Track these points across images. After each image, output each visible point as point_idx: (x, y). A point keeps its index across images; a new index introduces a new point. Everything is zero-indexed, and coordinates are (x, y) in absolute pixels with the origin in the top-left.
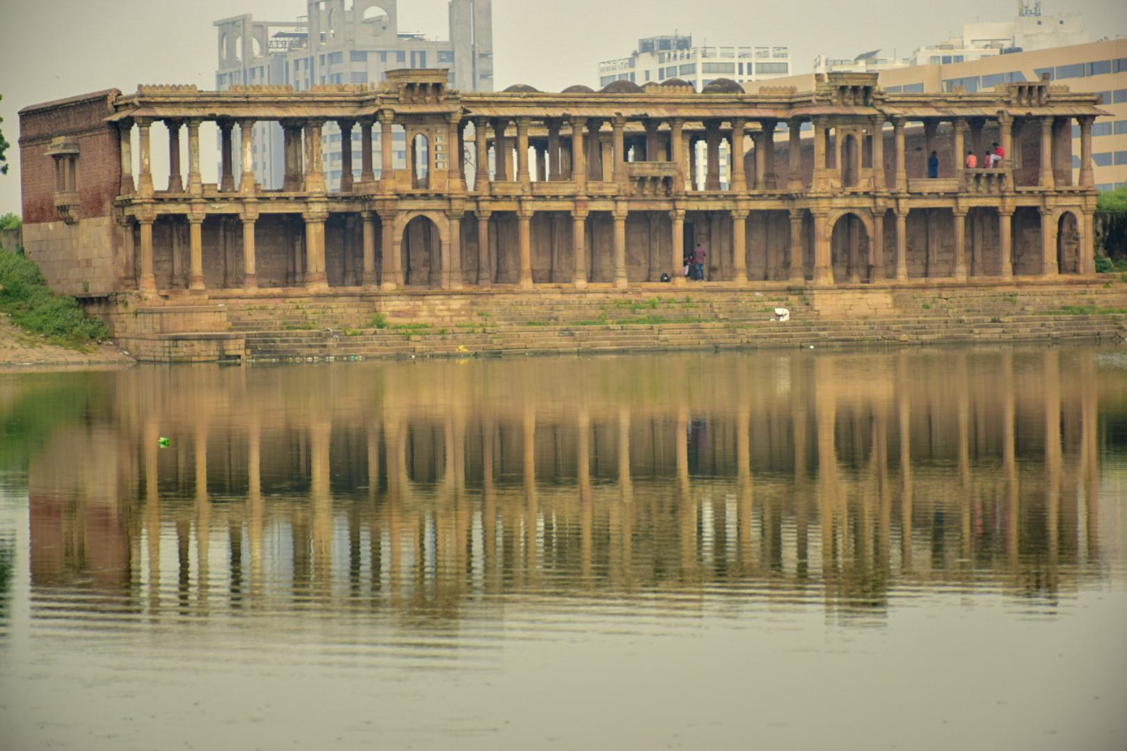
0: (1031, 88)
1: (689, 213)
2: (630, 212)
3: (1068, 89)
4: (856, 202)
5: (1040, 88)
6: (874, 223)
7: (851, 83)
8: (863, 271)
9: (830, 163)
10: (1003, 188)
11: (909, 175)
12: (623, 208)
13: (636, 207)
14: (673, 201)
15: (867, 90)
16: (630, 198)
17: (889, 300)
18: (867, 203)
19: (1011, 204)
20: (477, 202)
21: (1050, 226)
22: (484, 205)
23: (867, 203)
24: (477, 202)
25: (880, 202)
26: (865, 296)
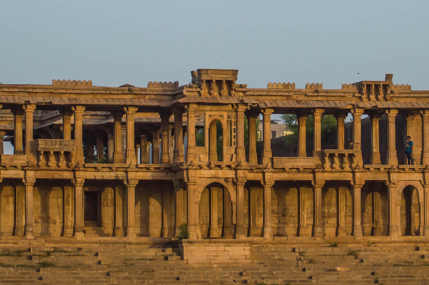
0: (377, 87)
1: (88, 182)
2: (37, 180)
3: (410, 87)
4: (220, 173)
5: (385, 87)
6: (237, 190)
7: (215, 77)
8: (181, 237)
9: (234, 144)
10: (354, 165)
11: (274, 155)
12: (31, 175)
13: (41, 175)
14: (74, 171)
15: (230, 83)
16: (37, 168)
17: (248, 253)
18: (230, 174)
19: (361, 178)
20: (126, 172)
21: (396, 196)
22: (131, 175)
23: (230, 174)
24: (126, 172)
25: (240, 173)
26: (228, 248)
